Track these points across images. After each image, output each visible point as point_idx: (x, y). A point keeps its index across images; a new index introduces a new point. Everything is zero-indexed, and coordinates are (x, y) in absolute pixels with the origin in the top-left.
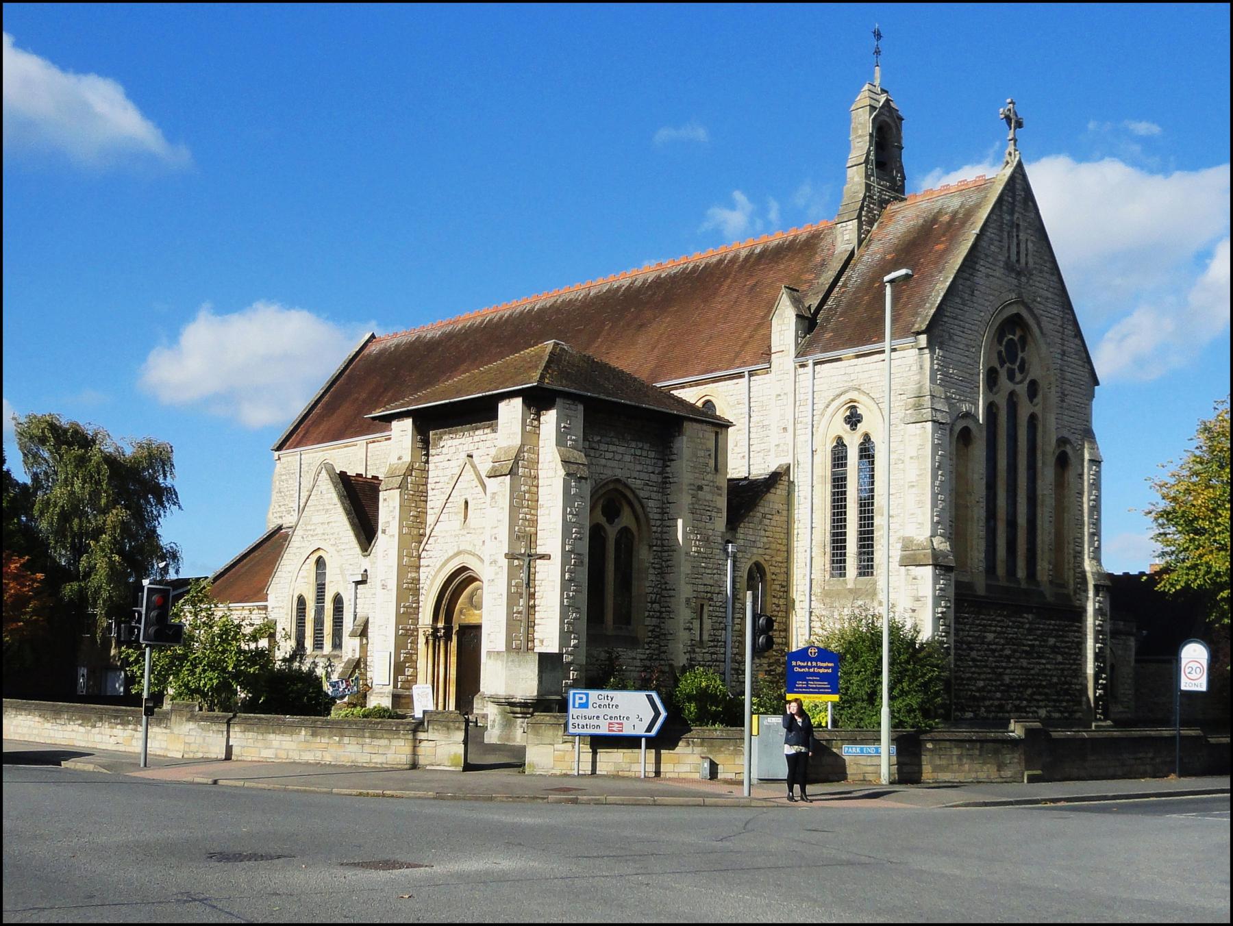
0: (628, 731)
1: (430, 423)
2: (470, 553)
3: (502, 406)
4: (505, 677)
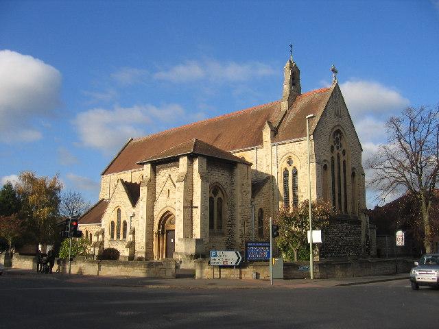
0: (229, 264)
1: (156, 165)
3: (180, 159)
4: (182, 247)
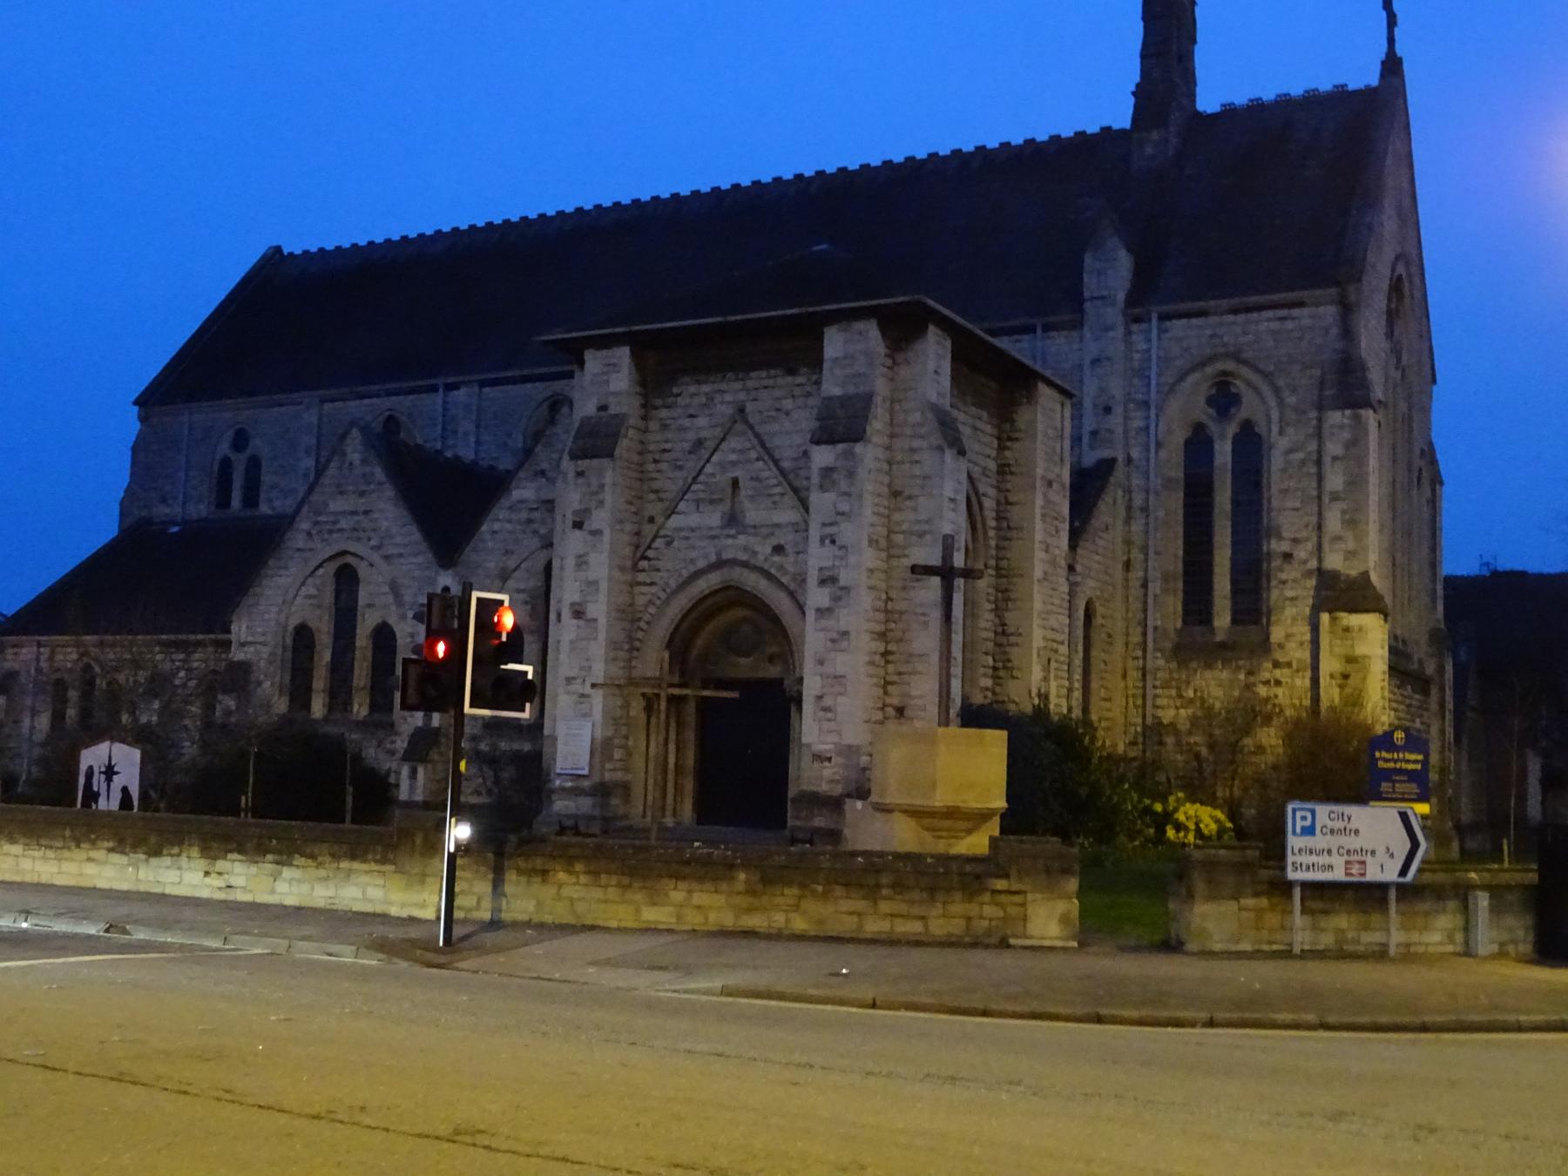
2: (745, 565)
